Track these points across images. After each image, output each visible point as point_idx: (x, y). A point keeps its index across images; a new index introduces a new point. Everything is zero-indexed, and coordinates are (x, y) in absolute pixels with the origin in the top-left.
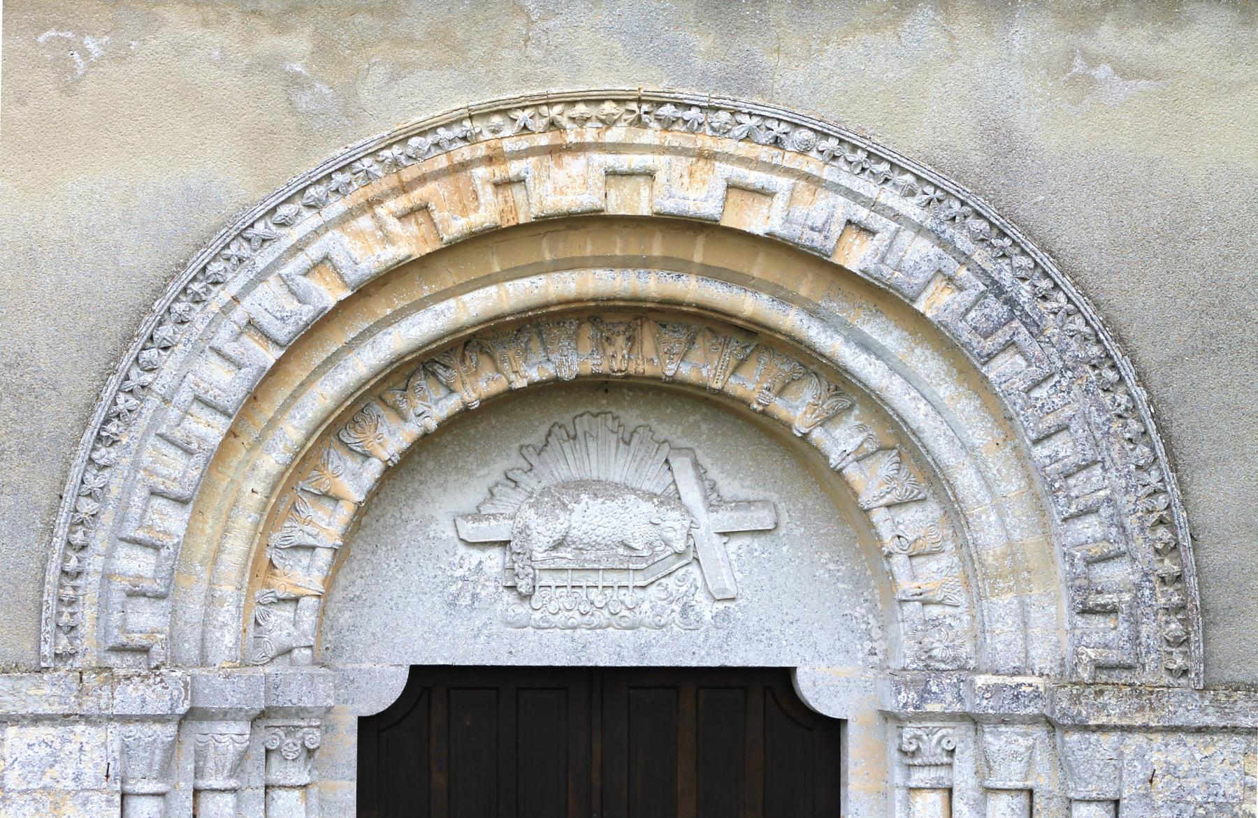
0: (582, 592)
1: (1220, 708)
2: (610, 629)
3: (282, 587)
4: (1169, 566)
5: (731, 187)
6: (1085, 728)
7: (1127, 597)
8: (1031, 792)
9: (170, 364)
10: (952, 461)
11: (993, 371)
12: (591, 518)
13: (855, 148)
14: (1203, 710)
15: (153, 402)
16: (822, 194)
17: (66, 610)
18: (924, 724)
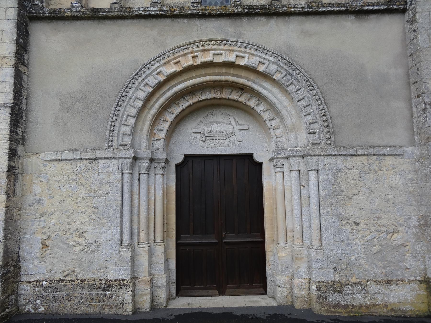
1: (338, 151)
3: (157, 137)
4: (326, 124)
5: (237, 56)
6: (311, 155)
7: (318, 130)
8: (299, 171)
9: (131, 91)
11: (289, 89)
12: (215, 127)
13: (260, 48)
14: (335, 151)
15: (128, 98)
16: (254, 57)
17: (111, 138)
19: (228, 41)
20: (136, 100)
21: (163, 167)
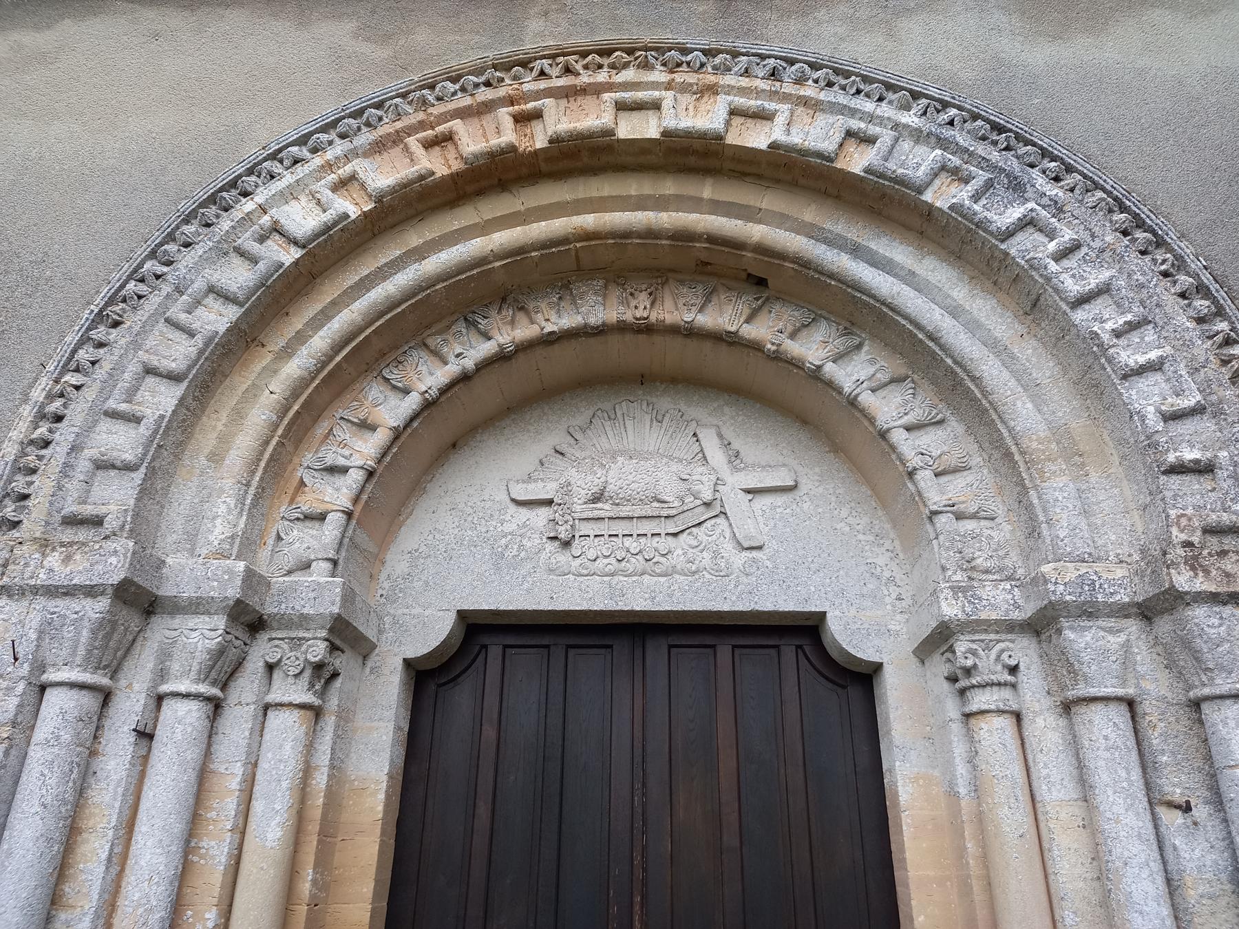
0: (618, 541)
2: (646, 577)
5: (734, 112)
8: (1131, 704)
9: (187, 259)
10: (976, 355)
15: (166, 289)
18: (977, 637)
19: (692, 51)
20: (210, 300)
21: (319, 667)
